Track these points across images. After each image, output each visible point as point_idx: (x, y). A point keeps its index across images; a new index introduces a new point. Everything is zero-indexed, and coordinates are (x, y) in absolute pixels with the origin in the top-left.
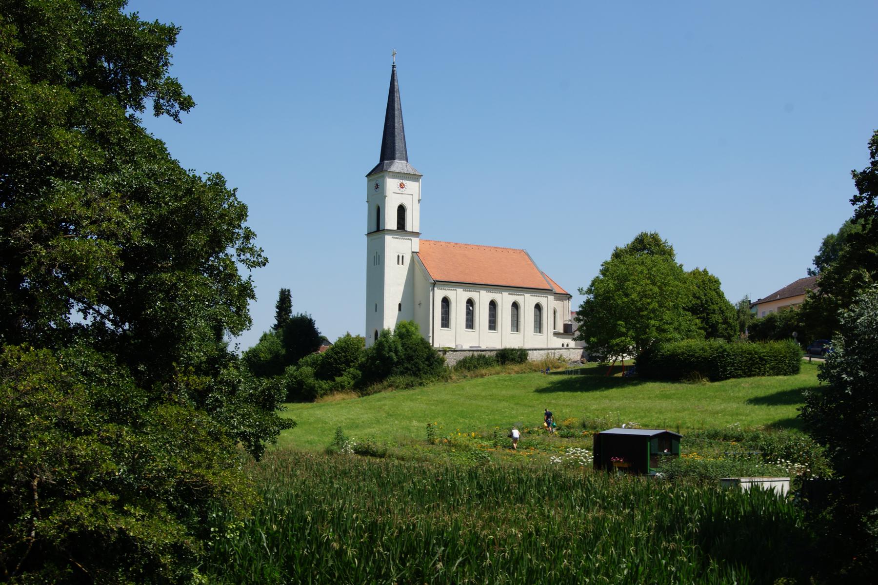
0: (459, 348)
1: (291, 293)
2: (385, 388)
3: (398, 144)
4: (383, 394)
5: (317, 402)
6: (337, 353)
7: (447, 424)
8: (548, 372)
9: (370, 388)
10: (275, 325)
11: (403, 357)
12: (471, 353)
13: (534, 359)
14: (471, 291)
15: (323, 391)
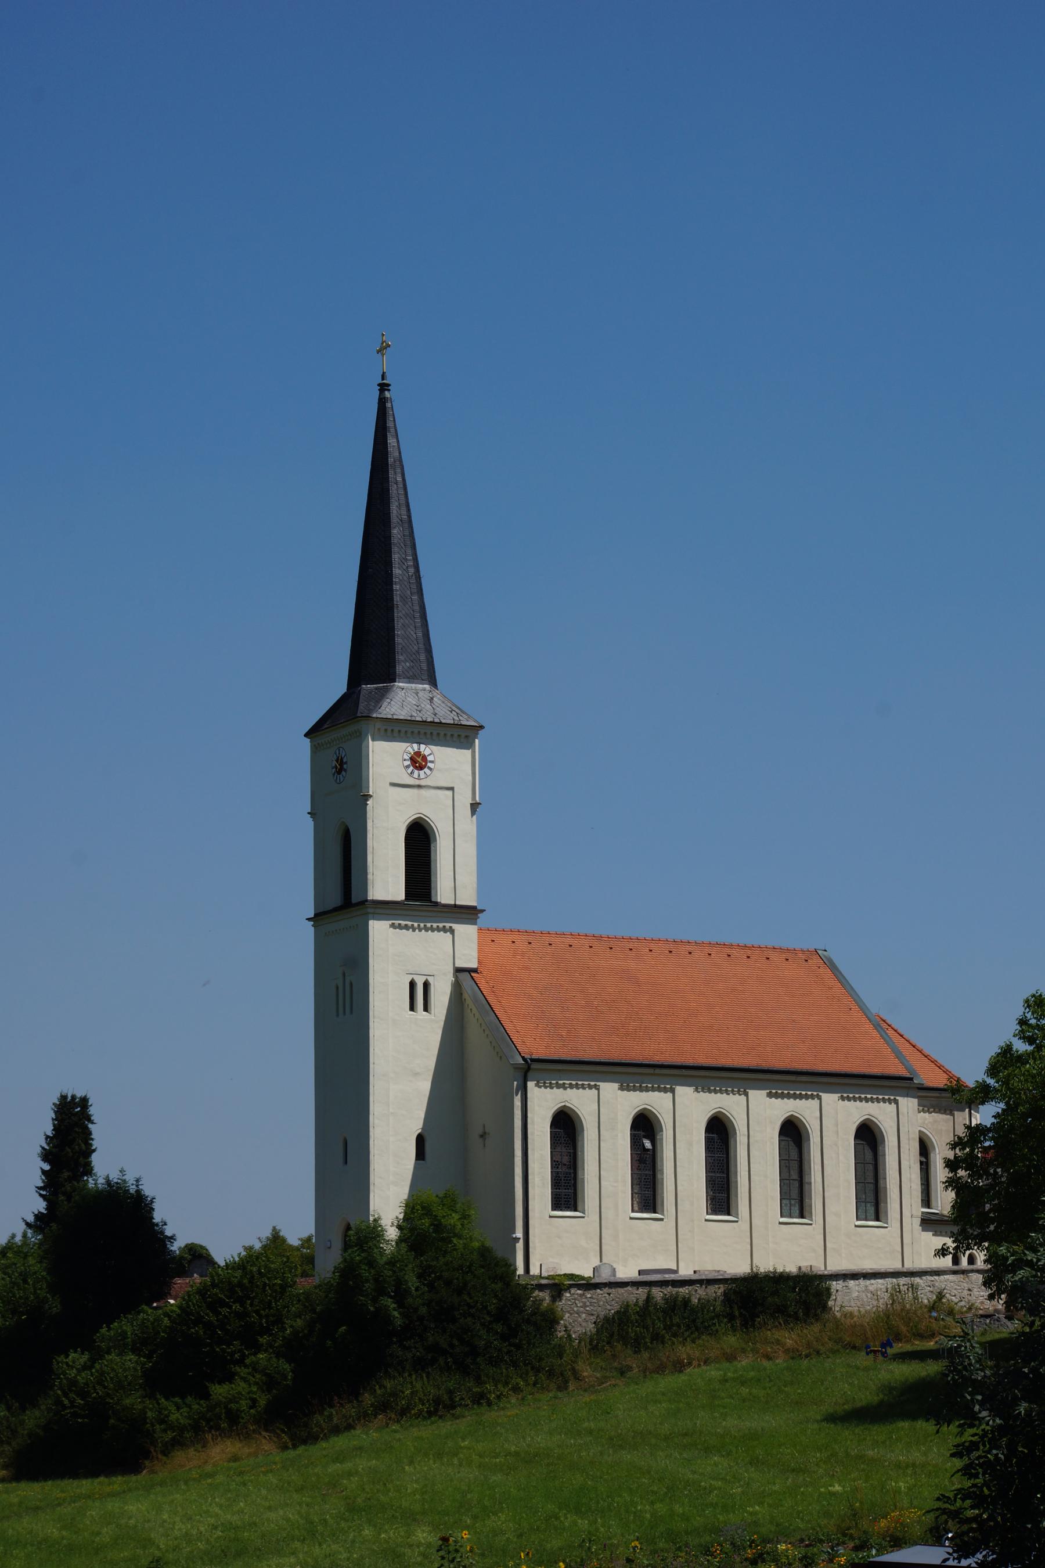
0: (605, 1276)
1: (92, 1111)
2: (365, 1415)
3: (404, 632)
4: (361, 1436)
5: (153, 1472)
6: (214, 1305)
7: (520, 1536)
8: (890, 1351)
9: (317, 1417)
10: (39, 1217)
11: (423, 1310)
12: (642, 1292)
13: (853, 1307)
14: (647, 1090)
15: (170, 1435)
